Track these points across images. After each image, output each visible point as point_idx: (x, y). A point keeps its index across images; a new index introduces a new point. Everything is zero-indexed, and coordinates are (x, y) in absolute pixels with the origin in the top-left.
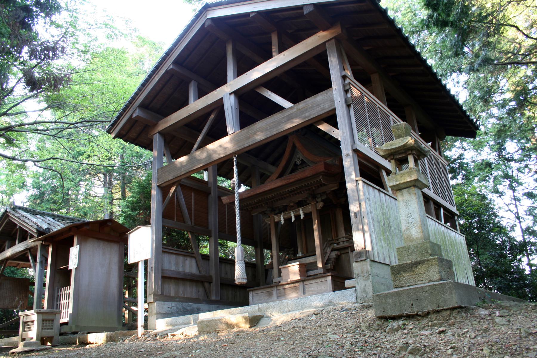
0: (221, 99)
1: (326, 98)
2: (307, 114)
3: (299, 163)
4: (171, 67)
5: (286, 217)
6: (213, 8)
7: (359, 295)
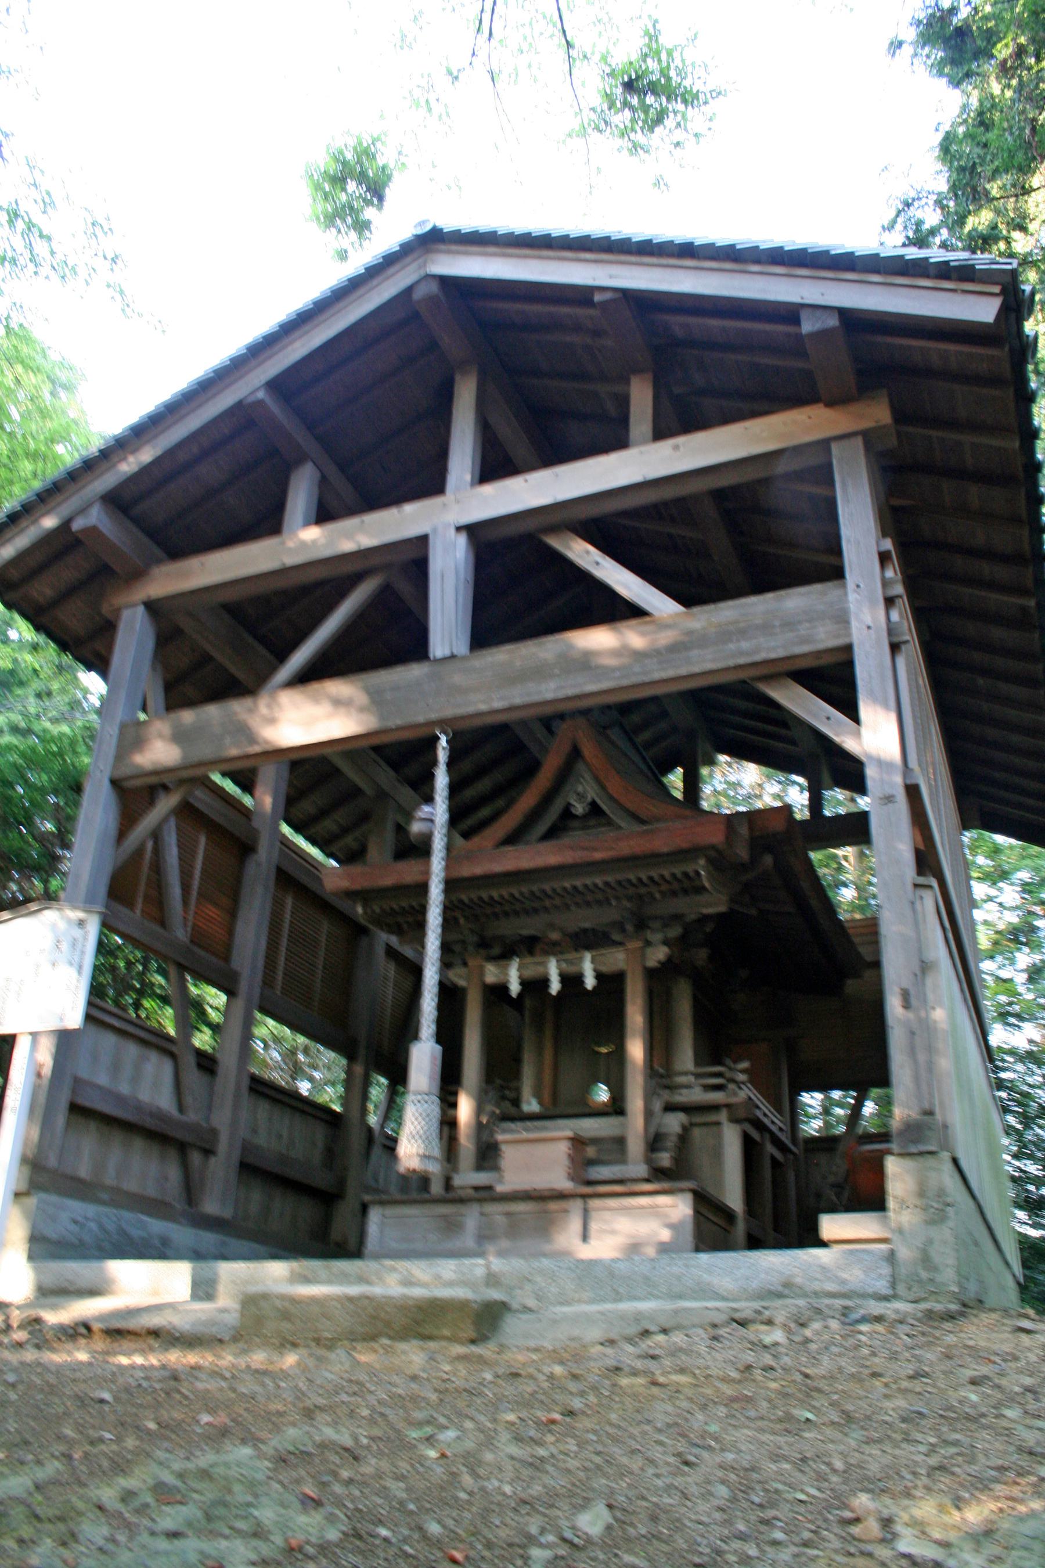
0: (423, 540)
1: (822, 607)
2: (745, 645)
3: (579, 809)
4: (261, 395)
5: (531, 972)
6: (454, 247)
7: (903, 1271)
